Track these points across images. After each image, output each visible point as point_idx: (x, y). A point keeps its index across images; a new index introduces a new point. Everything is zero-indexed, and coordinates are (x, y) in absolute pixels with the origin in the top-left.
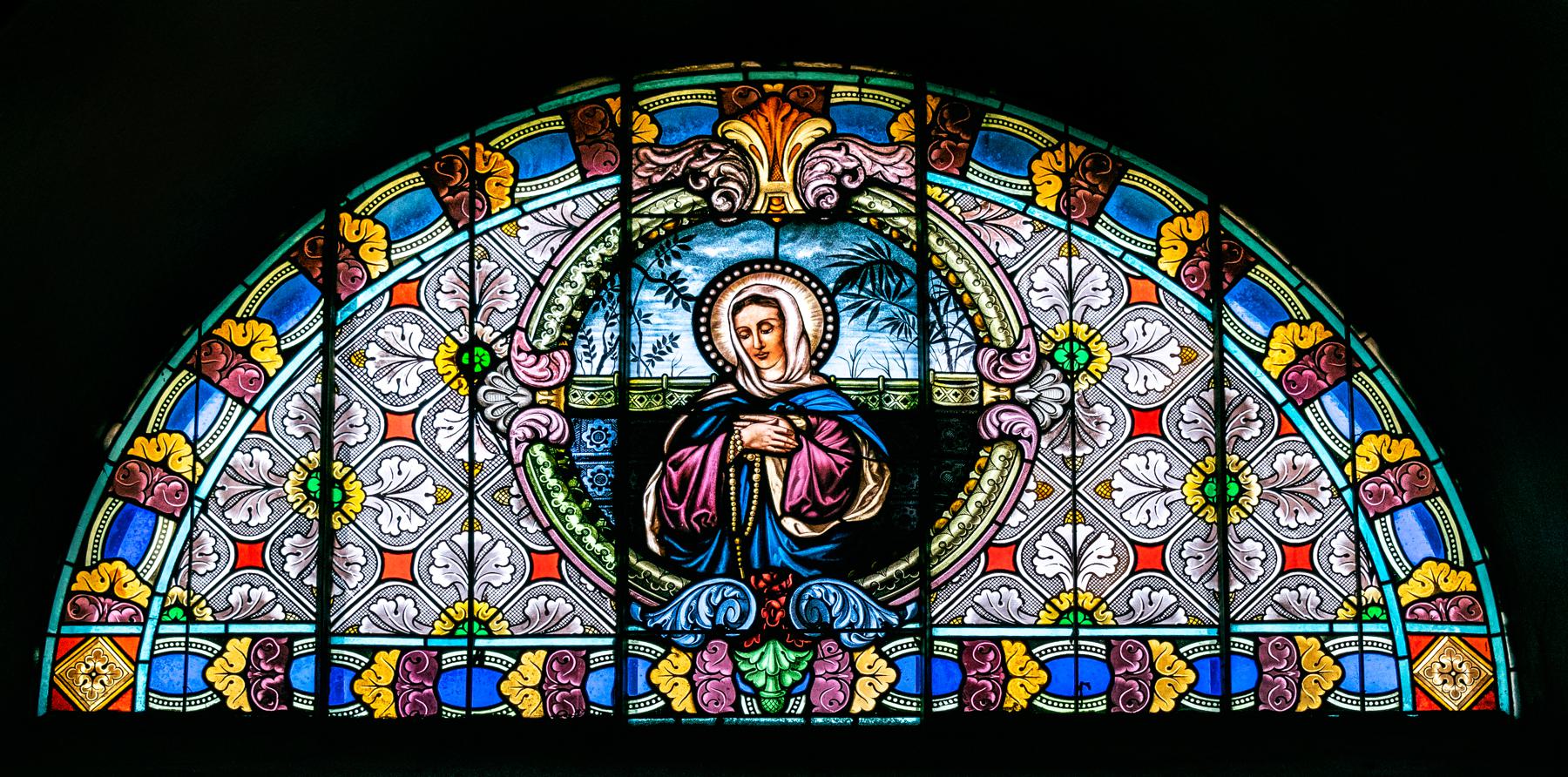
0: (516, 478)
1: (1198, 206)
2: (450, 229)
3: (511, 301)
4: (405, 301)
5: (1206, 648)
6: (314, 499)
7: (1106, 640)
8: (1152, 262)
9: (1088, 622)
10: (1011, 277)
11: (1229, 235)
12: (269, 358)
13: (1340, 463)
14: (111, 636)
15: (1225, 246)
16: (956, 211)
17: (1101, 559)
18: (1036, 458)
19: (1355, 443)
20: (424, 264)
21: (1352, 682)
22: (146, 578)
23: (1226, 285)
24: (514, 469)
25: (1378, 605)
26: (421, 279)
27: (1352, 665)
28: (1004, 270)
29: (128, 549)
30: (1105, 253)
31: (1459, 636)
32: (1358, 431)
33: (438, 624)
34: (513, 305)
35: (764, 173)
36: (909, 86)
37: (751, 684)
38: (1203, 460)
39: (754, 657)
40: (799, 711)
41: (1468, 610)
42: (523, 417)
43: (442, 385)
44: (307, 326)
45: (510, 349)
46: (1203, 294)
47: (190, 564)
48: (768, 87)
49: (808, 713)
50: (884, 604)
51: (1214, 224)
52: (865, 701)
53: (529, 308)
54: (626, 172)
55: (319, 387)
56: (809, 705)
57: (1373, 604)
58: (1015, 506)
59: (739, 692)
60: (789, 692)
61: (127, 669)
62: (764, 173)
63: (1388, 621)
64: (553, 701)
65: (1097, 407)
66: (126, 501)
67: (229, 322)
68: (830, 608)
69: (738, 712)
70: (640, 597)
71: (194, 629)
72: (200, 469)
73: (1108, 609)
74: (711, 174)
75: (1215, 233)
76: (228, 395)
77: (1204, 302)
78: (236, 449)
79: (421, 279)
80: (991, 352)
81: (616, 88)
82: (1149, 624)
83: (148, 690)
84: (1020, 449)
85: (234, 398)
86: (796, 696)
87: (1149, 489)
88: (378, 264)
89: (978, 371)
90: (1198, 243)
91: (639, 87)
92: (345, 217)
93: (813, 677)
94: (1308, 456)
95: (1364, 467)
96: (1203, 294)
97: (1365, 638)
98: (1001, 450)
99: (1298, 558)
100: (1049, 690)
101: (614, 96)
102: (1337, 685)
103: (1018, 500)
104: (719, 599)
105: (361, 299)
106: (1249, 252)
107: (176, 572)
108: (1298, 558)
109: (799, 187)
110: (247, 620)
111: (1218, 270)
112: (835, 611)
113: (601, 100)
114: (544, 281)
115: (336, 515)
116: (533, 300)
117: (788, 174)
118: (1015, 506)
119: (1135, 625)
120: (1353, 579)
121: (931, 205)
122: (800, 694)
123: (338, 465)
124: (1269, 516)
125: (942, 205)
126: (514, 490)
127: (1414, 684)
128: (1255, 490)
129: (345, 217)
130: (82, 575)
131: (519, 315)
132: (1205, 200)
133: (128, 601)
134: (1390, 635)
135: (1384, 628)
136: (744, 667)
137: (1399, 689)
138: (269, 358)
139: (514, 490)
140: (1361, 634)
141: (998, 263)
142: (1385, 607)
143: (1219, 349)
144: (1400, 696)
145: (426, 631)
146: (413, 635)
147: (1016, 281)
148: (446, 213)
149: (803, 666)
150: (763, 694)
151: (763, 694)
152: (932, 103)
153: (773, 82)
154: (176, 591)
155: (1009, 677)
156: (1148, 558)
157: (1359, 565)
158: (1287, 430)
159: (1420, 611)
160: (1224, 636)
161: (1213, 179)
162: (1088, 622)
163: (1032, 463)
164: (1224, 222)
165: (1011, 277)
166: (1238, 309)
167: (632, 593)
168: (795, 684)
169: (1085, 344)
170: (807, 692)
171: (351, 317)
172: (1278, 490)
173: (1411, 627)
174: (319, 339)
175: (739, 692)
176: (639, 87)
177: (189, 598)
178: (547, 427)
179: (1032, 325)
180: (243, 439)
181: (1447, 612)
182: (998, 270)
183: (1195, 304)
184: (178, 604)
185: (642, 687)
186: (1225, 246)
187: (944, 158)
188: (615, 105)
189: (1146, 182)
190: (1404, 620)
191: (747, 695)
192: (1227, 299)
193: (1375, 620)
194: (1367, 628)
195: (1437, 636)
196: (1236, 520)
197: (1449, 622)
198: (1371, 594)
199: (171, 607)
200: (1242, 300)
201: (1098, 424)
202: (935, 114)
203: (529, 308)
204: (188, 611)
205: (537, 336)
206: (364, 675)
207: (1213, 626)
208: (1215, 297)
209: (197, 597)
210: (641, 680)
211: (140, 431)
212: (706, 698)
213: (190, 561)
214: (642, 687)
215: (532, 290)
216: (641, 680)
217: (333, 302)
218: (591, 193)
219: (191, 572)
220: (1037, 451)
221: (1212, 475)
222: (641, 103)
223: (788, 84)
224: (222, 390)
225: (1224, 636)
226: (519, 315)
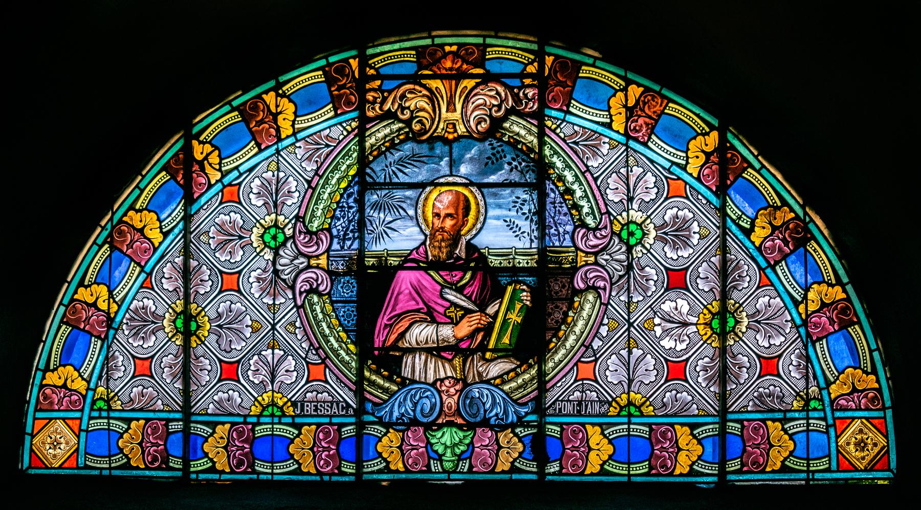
0: (299, 316)
1: (712, 128)
2: (256, 149)
3: (295, 199)
4: (230, 287)
5: (710, 429)
6: (180, 332)
7: (649, 425)
8: (684, 168)
9: (638, 413)
10: (596, 179)
11: (733, 147)
12: (155, 236)
13: (796, 304)
14: (64, 419)
15: (729, 155)
16: (562, 135)
17: (648, 369)
18: (609, 303)
19: (807, 289)
20: (241, 175)
21: (800, 452)
22: (85, 377)
23: (729, 182)
24: (298, 310)
25: (817, 399)
26: (240, 184)
27: (801, 438)
28: (592, 175)
29: (75, 358)
30: (652, 161)
31: (867, 419)
32: (810, 280)
33: (253, 408)
34: (295, 200)
35: (444, 109)
36: (534, 47)
37: (436, 452)
38: (621, 215)
39: (439, 434)
40: (465, 470)
41: (872, 400)
42: (303, 276)
43: (256, 395)
44: (174, 212)
45: (294, 232)
46: (714, 189)
47: (107, 373)
48: (447, 48)
49: (470, 471)
50: (515, 401)
51: (723, 139)
52: (503, 465)
53: (306, 201)
54: (361, 108)
55: (181, 257)
56: (471, 467)
57: (815, 398)
58: (595, 336)
59: (429, 458)
60: (460, 458)
61: (74, 440)
62: (444, 109)
63: (824, 410)
64: (321, 459)
65: (647, 269)
66: (74, 327)
67: (131, 213)
68: (484, 404)
69: (429, 471)
70: (371, 398)
71: (112, 414)
72: (114, 307)
73: (650, 405)
74: (412, 108)
75: (723, 147)
76: (132, 260)
77: (715, 194)
78: (134, 299)
79: (240, 184)
80: (583, 231)
81: (354, 53)
82: (675, 415)
83: (86, 453)
84: (600, 296)
85: (136, 262)
86: (463, 460)
87: (677, 323)
88: (215, 176)
89: (575, 245)
90: (711, 153)
91: (370, 51)
92: (195, 143)
93: (474, 447)
94: (778, 299)
95: (812, 307)
96: (714, 189)
97: (811, 421)
98: (591, 297)
99: (769, 365)
100: (614, 458)
101: (354, 57)
102: (791, 453)
103: (597, 332)
104: (417, 397)
105: (203, 200)
106: (745, 159)
107: (100, 377)
108: (769, 365)
109: (465, 119)
110: (141, 410)
111: (725, 171)
112: (488, 406)
113: (346, 60)
114: (313, 185)
115: (194, 338)
116: (308, 196)
117: (459, 106)
118: (595, 336)
119: (666, 416)
120: (803, 382)
121: (547, 131)
122: (466, 459)
123: (194, 306)
124: (660, 250)
125: (554, 131)
126: (298, 324)
127: (838, 452)
128: (745, 321)
129: (195, 143)
130: (48, 374)
131: (300, 207)
132: (715, 122)
133: (75, 391)
134: (824, 419)
135: (822, 414)
136: (433, 441)
137: (829, 456)
138: (155, 236)
139: (298, 324)
140: (808, 418)
141: (588, 170)
142: (821, 400)
143: (724, 228)
144: (830, 460)
145: (247, 412)
146: (239, 415)
147: (599, 183)
148: (254, 139)
149: (467, 441)
150: (444, 458)
151: (444, 458)
152: (549, 60)
153: (451, 45)
154: (100, 389)
155: (590, 449)
156: (676, 370)
157: (807, 372)
158: (764, 283)
159: (843, 402)
160: (723, 422)
161: (729, 113)
162: (638, 413)
163: (606, 305)
164: (730, 136)
165: (596, 179)
166: (738, 199)
167: (368, 396)
168: (463, 452)
169: (733, 314)
170: (470, 458)
171: (199, 210)
172: (758, 322)
173: (838, 414)
174: (181, 226)
175: (429, 458)
176: (370, 51)
177: (108, 394)
178: (317, 280)
179: (608, 213)
180: (137, 292)
181: (860, 402)
182: (588, 175)
183: (708, 194)
184: (101, 399)
185: (371, 453)
186: (729, 155)
187: (555, 100)
188: (354, 63)
189: (682, 110)
190: (833, 411)
191: (434, 459)
192: (732, 193)
193: (815, 409)
194: (811, 414)
195: (853, 418)
196: (732, 342)
197: (861, 410)
198: (813, 389)
199: (97, 399)
200: (737, 192)
201: (647, 280)
202: (550, 70)
203: (306, 201)
204: (108, 401)
205: (310, 222)
206: (209, 440)
207: (714, 416)
208: (722, 191)
209: (112, 394)
210: (371, 449)
211: (81, 284)
212: (410, 461)
213: (108, 371)
214: (371, 453)
215: (307, 191)
216: (371, 449)
217: (189, 200)
218: (340, 124)
219: (108, 380)
220: (609, 298)
221: (717, 314)
222: (370, 62)
223: (460, 45)
224: (128, 256)
225: (723, 422)
226: (300, 207)
